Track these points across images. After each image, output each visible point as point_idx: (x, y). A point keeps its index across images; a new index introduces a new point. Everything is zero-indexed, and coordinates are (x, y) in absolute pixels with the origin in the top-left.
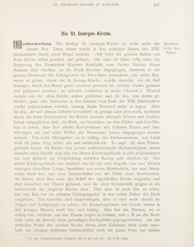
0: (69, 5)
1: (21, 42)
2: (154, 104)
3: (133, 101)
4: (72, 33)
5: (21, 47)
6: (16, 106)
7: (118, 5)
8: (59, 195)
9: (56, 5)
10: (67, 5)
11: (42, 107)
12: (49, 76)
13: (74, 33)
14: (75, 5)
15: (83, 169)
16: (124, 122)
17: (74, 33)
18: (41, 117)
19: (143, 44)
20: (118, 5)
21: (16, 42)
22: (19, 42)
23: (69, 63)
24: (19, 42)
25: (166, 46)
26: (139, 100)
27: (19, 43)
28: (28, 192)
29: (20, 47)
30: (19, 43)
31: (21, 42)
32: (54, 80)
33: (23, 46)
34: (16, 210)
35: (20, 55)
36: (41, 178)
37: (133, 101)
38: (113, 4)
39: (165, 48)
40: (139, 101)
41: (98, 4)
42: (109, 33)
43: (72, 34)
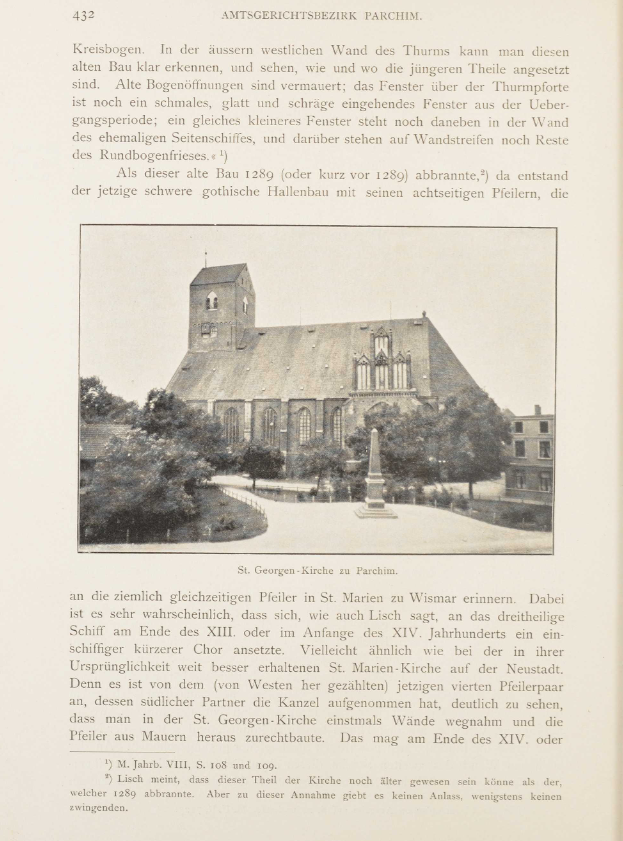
3: (227, 633)
7: (415, 16)
16: (506, 688)
20: (415, 16)
23: (283, 696)
28: (528, 626)
34: (182, 686)
36: (87, 64)
37: (227, 633)
38: (401, 16)
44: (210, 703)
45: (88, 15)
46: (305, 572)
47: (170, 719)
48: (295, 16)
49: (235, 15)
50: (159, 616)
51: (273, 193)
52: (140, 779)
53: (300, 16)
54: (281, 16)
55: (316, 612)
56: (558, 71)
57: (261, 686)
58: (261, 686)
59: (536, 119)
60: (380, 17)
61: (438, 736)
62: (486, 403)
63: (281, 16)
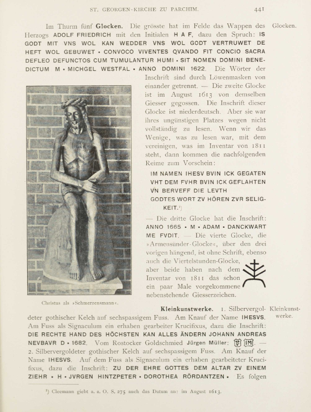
0: (115, 10)
6: (245, 127)
9: (94, 10)
10: (112, 10)
11: (192, 155)
12: (237, 95)
14: (126, 9)
16: (206, 121)
20: (195, 9)
32: (159, 136)
38: (188, 9)
41: (163, 9)
50: (160, 35)
51: (27, 36)
52: (220, 270)
60: (178, 10)
61: (239, 375)
62: (129, 226)
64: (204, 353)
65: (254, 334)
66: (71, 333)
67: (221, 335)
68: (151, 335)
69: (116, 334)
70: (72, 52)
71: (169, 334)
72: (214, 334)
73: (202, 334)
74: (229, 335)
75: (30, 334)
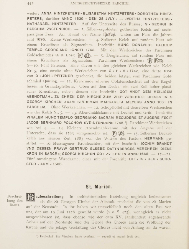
1: (34, 194)
2: (82, 84)
4: (87, 186)
5: (34, 200)
7: (127, 4)
8: (162, 113)
13: (90, 186)
15: (140, 113)
17: (90, 186)
18: (126, 77)
19: (78, 197)
20: (127, 4)
21: (29, 195)
22: (32, 194)
24: (32, 194)
25: (10, 199)
26: (162, 34)
27: (32, 196)
29: (33, 199)
30: (32, 196)
31: (34, 194)
33: (36, 199)
35: (132, 218)
39: (8, 201)
40: (162, 35)
42: (109, 187)
43: (87, 187)
44: (157, 50)
45: (31, 3)
46: (41, 164)
47: (99, 217)
48: (92, 3)
49: (75, 3)
50: (31, 40)
53: (94, 3)
54: (88, 3)
55: (29, 127)
56: (123, 77)
57: (132, 66)
58: (132, 66)
59: (121, 49)
60: (117, 4)
63: (88, 3)
64: (144, 35)
65: (150, 45)
66: (54, 23)
67: (54, 123)
68: (62, 50)
69: (146, 144)
70: (100, 149)
71: (37, 117)
72: (46, 76)
73: (152, 138)
74: (66, 19)
75: (149, 97)
